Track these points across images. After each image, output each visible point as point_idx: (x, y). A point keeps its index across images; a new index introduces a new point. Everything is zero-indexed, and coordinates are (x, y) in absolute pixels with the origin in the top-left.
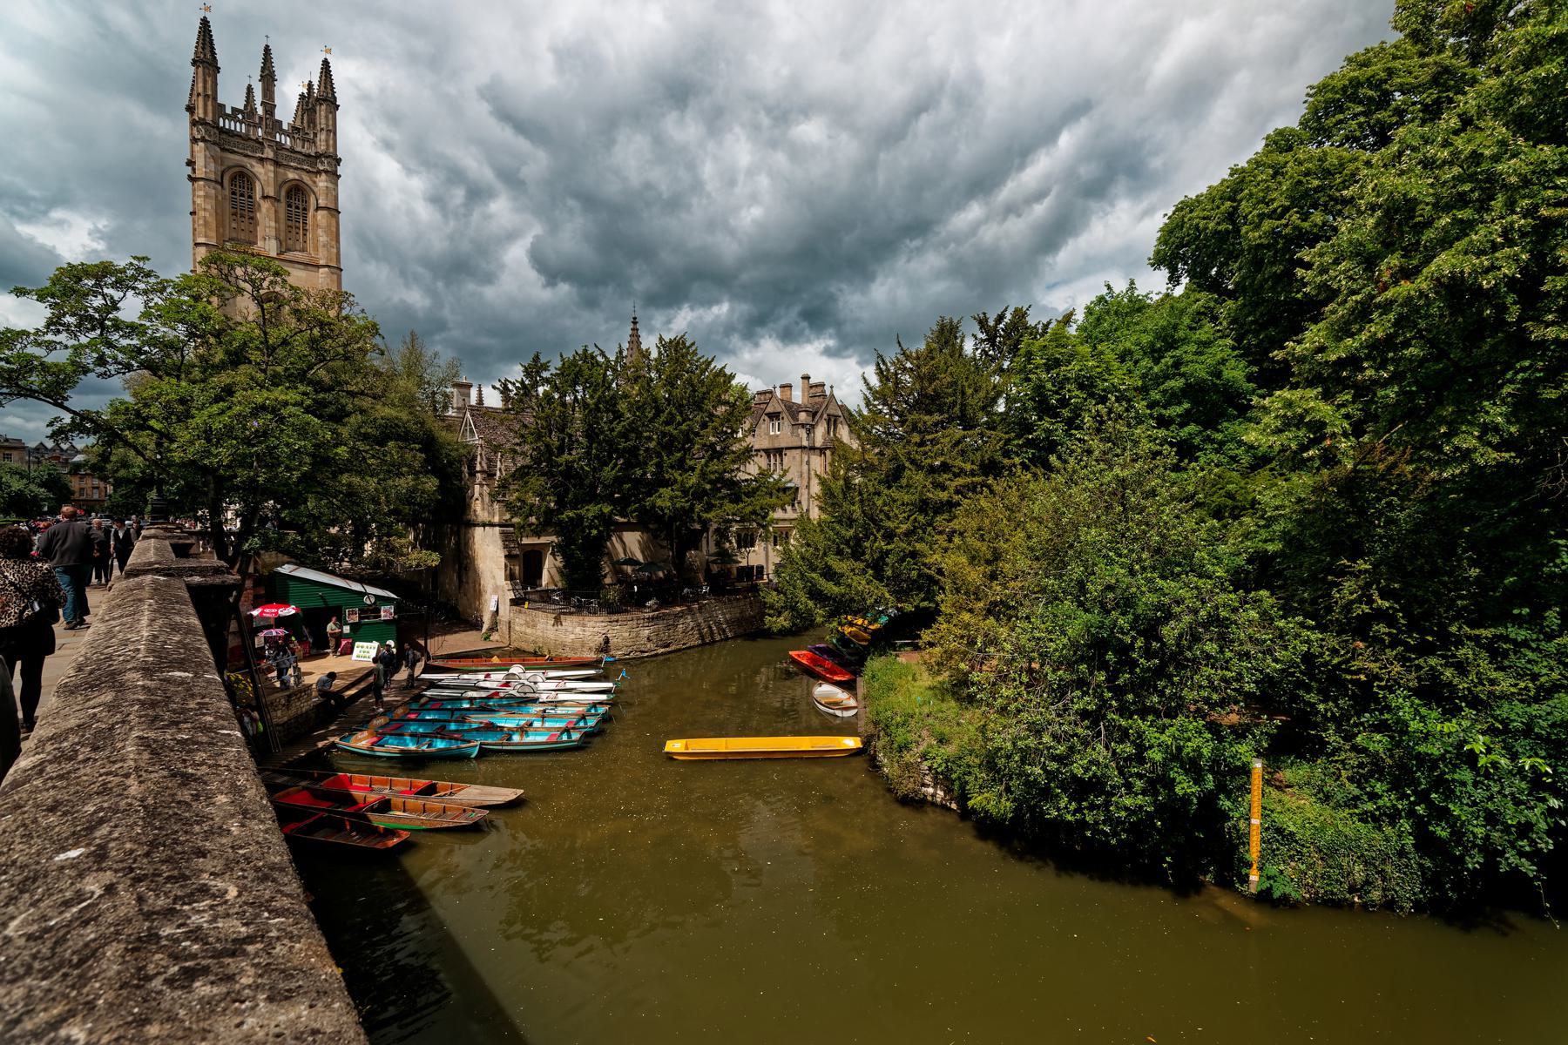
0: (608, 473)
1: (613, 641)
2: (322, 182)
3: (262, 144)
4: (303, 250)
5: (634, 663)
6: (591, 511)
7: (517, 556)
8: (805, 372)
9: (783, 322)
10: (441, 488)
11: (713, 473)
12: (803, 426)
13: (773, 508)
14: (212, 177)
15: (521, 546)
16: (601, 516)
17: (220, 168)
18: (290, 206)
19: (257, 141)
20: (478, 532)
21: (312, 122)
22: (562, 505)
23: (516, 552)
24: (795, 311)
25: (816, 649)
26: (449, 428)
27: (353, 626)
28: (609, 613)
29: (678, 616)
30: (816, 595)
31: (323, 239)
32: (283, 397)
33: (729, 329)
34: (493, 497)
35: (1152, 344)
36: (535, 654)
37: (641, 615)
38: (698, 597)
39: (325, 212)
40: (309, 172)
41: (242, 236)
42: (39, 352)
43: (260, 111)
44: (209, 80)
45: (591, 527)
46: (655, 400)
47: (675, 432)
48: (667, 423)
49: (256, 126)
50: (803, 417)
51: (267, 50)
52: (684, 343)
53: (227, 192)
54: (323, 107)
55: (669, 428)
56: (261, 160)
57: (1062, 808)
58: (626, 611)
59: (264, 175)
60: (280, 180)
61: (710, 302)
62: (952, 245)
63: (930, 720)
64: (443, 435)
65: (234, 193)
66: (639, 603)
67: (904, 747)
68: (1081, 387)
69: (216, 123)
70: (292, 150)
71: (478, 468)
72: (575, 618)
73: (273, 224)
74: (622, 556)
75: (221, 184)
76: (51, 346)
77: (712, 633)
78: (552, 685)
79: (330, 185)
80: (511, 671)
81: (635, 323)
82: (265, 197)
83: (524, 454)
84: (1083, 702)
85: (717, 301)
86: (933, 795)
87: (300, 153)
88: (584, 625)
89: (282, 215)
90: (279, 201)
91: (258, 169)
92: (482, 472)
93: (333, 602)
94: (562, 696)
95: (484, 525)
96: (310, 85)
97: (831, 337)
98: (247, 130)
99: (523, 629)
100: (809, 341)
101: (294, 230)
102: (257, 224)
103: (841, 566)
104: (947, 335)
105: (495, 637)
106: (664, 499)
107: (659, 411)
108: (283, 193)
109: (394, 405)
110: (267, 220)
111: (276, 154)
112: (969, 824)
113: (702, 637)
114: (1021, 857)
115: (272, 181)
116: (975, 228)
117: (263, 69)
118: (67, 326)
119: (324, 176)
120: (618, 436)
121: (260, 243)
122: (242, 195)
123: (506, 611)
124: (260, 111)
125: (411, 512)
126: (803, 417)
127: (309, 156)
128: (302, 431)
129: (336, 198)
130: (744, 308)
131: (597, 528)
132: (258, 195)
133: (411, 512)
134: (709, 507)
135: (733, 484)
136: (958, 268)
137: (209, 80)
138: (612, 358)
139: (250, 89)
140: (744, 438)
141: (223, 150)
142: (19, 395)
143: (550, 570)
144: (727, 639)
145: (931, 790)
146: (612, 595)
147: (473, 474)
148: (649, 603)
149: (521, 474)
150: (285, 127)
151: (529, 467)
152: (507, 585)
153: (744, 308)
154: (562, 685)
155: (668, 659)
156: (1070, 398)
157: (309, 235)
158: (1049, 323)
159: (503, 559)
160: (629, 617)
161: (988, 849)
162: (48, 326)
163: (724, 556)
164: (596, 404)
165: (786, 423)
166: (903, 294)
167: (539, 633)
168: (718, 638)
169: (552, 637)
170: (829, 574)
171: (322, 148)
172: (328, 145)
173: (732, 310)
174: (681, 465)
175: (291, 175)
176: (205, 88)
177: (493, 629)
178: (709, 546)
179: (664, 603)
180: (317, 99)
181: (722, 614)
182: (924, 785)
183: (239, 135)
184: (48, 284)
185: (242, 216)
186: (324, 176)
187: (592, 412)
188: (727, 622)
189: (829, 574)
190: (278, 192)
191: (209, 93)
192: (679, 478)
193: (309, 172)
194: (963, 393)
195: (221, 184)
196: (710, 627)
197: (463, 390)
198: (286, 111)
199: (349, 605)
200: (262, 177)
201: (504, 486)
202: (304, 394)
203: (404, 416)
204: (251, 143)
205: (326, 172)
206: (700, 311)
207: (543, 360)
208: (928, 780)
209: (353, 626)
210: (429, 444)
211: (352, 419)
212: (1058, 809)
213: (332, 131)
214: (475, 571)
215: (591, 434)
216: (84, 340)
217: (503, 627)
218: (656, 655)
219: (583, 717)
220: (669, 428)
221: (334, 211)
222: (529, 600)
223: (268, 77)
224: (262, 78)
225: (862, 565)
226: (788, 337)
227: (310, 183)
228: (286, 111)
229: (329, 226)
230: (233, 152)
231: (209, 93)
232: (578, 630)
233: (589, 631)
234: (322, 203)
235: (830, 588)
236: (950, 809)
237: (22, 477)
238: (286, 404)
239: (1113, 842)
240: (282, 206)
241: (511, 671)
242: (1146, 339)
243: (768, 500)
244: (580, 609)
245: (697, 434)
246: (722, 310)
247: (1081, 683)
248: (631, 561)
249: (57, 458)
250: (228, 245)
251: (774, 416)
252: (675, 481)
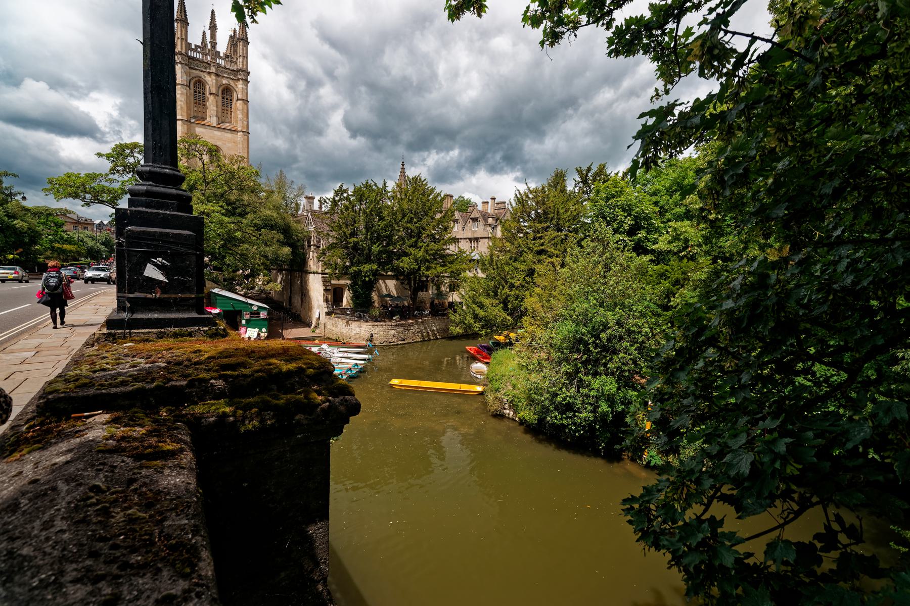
0: (375, 248)
1: (375, 336)
2: (240, 85)
4: (230, 122)
5: (386, 347)
6: (366, 267)
7: (329, 290)
8: (493, 196)
9: (491, 163)
10: (293, 253)
11: (432, 250)
12: (490, 225)
13: (464, 270)
14: (185, 83)
15: (331, 285)
16: (371, 270)
17: (189, 78)
18: (223, 98)
19: (207, 63)
20: (311, 276)
21: (235, 51)
22: (352, 264)
23: (329, 288)
24: (498, 157)
25: (481, 346)
26: (298, 222)
27: (247, 320)
28: (375, 321)
29: (410, 325)
30: (476, 317)
31: (240, 116)
32: (212, 208)
33: (460, 166)
34: (318, 259)
35: (671, 187)
36: (336, 340)
37: (390, 323)
38: (422, 316)
39: (241, 102)
40: (233, 79)
41: (199, 115)
42: (107, 184)
43: (209, 46)
44: (183, 30)
45: (365, 276)
46: (403, 210)
47: (413, 228)
48: (408, 222)
49: (207, 55)
50: (490, 221)
51: (213, 12)
52: (420, 179)
53: (192, 91)
54: (241, 43)
55: (409, 225)
56: (209, 73)
57: (554, 417)
58: (384, 321)
59: (211, 81)
60: (219, 84)
61: (448, 149)
62: (597, 115)
63: (512, 379)
64: (295, 225)
65: (195, 92)
66: (391, 318)
67: (497, 390)
68: (624, 210)
69: (187, 53)
70: (225, 68)
71: (312, 243)
72: (356, 323)
73: (215, 108)
74: (385, 292)
75: (189, 87)
76: (112, 181)
77: (428, 335)
78: (341, 355)
79: (244, 87)
80: (322, 347)
81: (403, 165)
82: (211, 94)
83: (333, 237)
84: (565, 367)
85: (452, 149)
86: (509, 414)
88: (361, 327)
89: (220, 104)
90: (218, 96)
92: (314, 245)
93: (237, 308)
94: (344, 360)
95: (314, 273)
96: (235, 31)
97: (518, 170)
98: (203, 57)
99: (331, 327)
100: (506, 173)
101: (225, 112)
102: (207, 109)
103: (487, 302)
104: (559, 178)
105: (317, 331)
106: (405, 263)
107: (404, 215)
108: (220, 92)
109: (270, 209)
110: (212, 105)
111: (217, 70)
112: (522, 427)
113: (423, 337)
114: (540, 441)
115: (214, 84)
116: (610, 104)
117: (211, 23)
118: (118, 171)
119: (241, 81)
120: (381, 229)
121: (208, 119)
122: (199, 93)
123: (323, 316)
124: (209, 46)
125: (273, 264)
126: (490, 221)
127: (234, 71)
128: (221, 224)
129: (247, 94)
130: (468, 153)
131: (368, 277)
132: (207, 93)
133: (273, 264)
134: (428, 269)
135: (443, 257)
136: (598, 129)
137: (183, 30)
138: (381, 186)
139: (204, 33)
140: (456, 230)
141: (190, 68)
142: (98, 203)
143: (347, 299)
144: (437, 339)
145: (508, 411)
146: (376, 312)
147: (309, 246)
148: (394, 318)
149: (332, 247)
150: (222, 55)
151: (336, 244)
152: (324, 305)
153: (468, 153)
154: (346, 355)
155: (404, 347)
156: (618, 216)
157: (233, 114)
158: (618, 173)
159: (322, 291)
160: (384, 324)
161: (528, 438)
162: (110, 171)
163: (440, 294)
164: (371, 211)
165: (481, 223)
166: (563, 146)
167: (338, 330)
168: (432, 338)
169: (345, 332)
170: (481, 306)
171: (240, 66)
172: (243, 65)
173: (460, 154)
174: (414, 245)
175: (225, 81)
176: (181, 34)
177: (317, 327)
178: (432, 291)
179: (403, 317)
180: (238, 39)
181: (434, 325)
182: (505, 409)
183: (198, 60)
184: (111, 151)
185: (200, 104)
186: (241, 81)
187: (369, 216)
188: (437, 330)
189: (481, 306)
190: (218, 91)
191: (184, 37)
192: (413, 252)
193: (233, 79)
194: (558, 212)
195: (189, 87)
196: (428, 332)
197: (311, 201)
198: (222, 46)
199: (246, 310)
201: (324, 253)
202: (221, 206)
203: (275, 215)
204: (204, 64)
205: (242, 79)
206: (442, 155)
207: (345, 187)
208: (507, 406)
209: (247, 320)
210: (286, 231)
211: (249, 216)
212: (551, 417)
213: (246, 57)
214: (309, 297)
215: (367, 228)
216: (126, 178)
217: (321, 326)
218: (397, 345)
219: (350, 369)
220: (409, 225)
221: (246, 101)
222: (335, 313)
223: (213, 27)
224: (210, 28)
225: (497, 301)
226: (494, 170)
227: (233, 85)
228: (222, 46)
229: (243, 109)
230: (195, 69)
231: (184, 37)
232: (358, 329)
233: (363, 330)
234: (240, 97)
235: (481, 313)
236: (515, 420)
237: (93, 240)
238: (214, 211)
239: (577, 434)
240: (220, 98)
241: (322, 347)
242: (668, 184)
243: (464, 266)
244: (360, 318)
245: (424, 229)
246: (455, 153)
247: (566, 359)
248: (389, 295)
249: (109, 230)
250: (193, 120)
251: (475, 220)
252: (411, 254)
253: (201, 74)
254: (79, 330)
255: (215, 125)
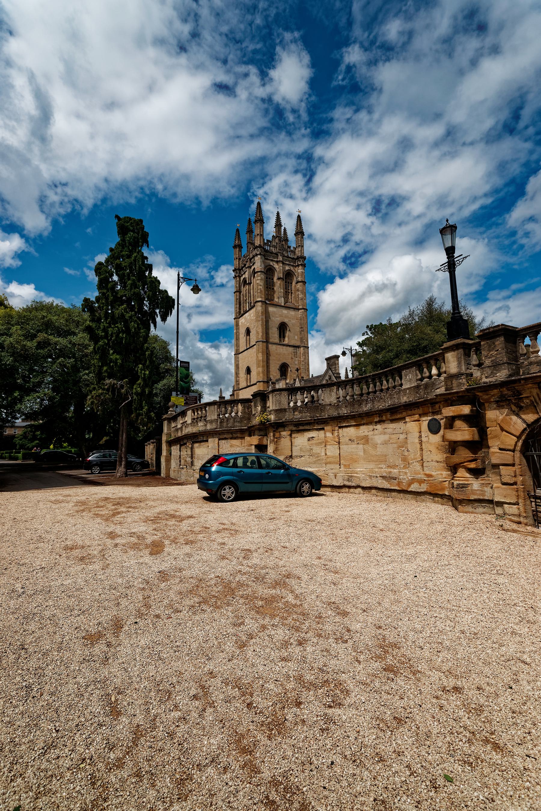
3: (277, 255)
14: (263, 270)
18: (286, 282)
39: (301, 284)
51: (278, 214)
56: (277, 262)
79: (303, 271)
82: (279, 279)
87: (290, 258)
91: (276, 266)
119: (300, 267)
197: (246, 404)
200: (277, 270)
204: (273, 255)
253: (271, 263)
254: (424, 439)
255: (283, 304)
